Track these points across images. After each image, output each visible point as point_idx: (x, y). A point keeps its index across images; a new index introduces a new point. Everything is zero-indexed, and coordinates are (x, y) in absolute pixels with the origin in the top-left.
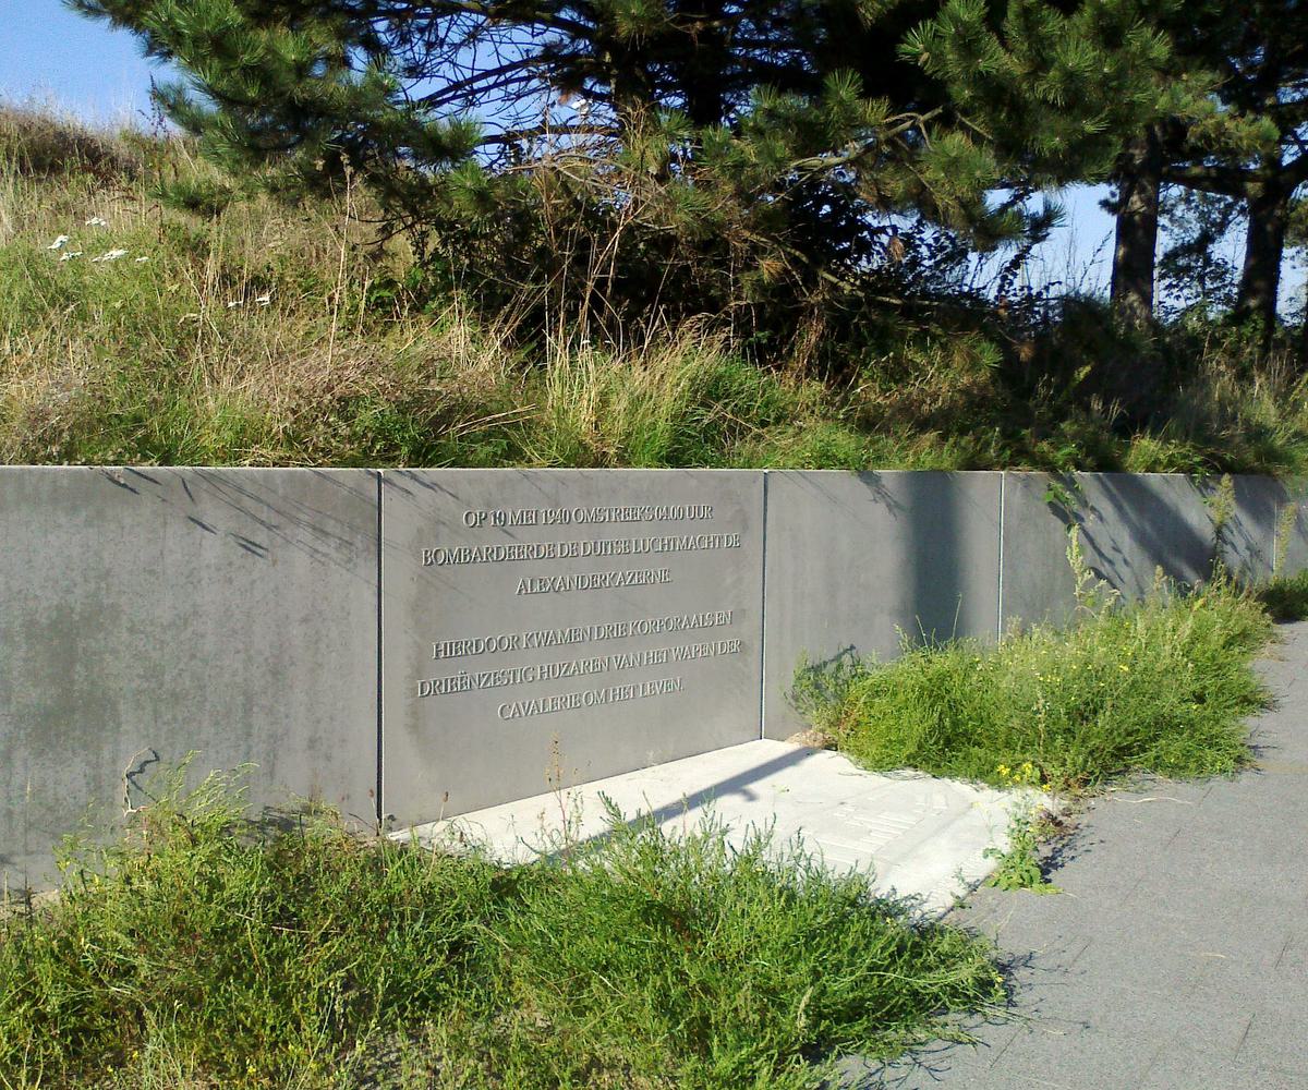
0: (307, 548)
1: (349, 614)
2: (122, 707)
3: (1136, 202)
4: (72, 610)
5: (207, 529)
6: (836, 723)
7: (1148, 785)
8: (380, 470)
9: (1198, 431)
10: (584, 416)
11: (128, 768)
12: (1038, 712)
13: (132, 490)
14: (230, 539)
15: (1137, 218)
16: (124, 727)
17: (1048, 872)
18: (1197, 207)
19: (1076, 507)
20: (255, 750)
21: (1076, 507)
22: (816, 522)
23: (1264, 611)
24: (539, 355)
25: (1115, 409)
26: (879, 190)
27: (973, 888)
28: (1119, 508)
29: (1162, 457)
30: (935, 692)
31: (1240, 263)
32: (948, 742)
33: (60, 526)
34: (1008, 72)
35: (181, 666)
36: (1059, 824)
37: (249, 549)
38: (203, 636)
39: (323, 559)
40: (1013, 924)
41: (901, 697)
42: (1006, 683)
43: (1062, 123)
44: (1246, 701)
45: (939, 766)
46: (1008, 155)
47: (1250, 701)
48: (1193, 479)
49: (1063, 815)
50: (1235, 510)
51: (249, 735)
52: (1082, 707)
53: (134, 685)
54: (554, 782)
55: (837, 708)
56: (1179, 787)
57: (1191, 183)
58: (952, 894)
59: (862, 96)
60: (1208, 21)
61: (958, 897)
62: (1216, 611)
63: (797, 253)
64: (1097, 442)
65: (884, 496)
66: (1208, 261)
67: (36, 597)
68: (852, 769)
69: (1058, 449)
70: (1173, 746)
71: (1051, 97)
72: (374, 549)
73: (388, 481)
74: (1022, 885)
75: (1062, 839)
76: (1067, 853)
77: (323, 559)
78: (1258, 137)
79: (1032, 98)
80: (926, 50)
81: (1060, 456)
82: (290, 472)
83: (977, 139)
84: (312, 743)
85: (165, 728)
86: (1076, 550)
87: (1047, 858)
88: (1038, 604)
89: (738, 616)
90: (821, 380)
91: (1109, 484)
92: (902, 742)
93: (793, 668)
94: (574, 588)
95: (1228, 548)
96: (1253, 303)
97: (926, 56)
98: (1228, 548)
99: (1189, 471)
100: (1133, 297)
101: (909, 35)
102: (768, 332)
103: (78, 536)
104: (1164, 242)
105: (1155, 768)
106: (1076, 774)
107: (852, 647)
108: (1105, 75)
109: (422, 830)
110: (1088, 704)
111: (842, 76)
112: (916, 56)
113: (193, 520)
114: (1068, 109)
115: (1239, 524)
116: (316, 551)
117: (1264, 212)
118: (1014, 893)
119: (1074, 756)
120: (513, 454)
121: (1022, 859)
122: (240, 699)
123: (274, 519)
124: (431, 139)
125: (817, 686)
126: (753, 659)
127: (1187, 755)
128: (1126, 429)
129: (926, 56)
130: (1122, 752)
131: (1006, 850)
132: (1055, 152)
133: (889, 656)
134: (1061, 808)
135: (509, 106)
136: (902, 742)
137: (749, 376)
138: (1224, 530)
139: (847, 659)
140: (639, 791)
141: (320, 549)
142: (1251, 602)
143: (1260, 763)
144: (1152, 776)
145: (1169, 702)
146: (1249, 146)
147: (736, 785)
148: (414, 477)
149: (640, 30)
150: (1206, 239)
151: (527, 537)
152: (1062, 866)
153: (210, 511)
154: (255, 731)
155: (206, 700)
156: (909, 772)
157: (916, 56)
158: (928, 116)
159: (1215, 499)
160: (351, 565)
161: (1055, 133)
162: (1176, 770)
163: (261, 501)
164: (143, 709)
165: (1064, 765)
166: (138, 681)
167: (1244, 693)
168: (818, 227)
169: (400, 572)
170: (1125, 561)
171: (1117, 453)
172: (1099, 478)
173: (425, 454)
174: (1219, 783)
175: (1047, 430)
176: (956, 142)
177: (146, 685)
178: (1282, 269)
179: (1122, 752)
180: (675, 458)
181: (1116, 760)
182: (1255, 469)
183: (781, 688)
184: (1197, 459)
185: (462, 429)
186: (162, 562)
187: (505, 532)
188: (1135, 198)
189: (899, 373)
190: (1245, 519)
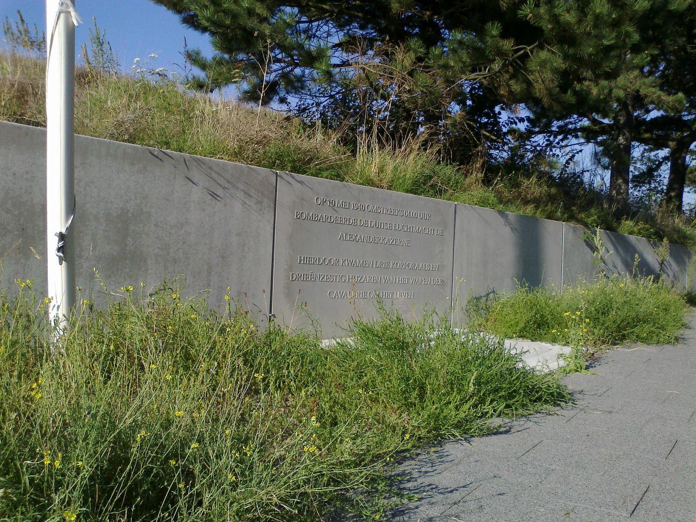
2: (149, 262)
4: (128, 211)
13: (160, 160)
14: (205, 190)
15: (621, 146)
16: (149, 271)
18: (646, 163)
34: (568, 21)
37: (213, 196)
40: (571, 383)
48: (649, 241)
50: (668, 258)
53: (155, 252)
60: (657, 27)
63: (472, 123)
65: (510, 224)
67: (112, 202)
69: (589, 218)
72: (272, 206)
73: (281, 177)
74: (577, 371)
77: (248, 208)
78: (676, 101)
80: (531, 12)
81: (590, 220)
82: (235, 165)
90: (482, 173)
94: (365, 241)
96: (673, 194)
97: (531, 15)
99: (648, 237)
102: (460, 151)
111: (493, 24)
112: (526, 16)
113: (187, 178)
116: (246, 203)
120: (339, 177)
122: (206, 267)
123: (227, 185)
124: (307, 52)
126: (448, 289)
129: (531, 15)
132: (590, 55)
133: (509, 292)
137: (448, 170)
141: (247, 202)
146: (673, 105)
148: (293, 177)
153: (196, 175)
154: (212, 284)
157: (526, 16)
158: (531, 47)
160: (261, 212)
162: (644, 340)
163: (221, 176)
164: (159, 264)
166: (157, 250)
169: (284, 218)
171: (615, 225)
173: (295, 170)
176: (544, 55)
178: (684, 195)
187: (334, 209)
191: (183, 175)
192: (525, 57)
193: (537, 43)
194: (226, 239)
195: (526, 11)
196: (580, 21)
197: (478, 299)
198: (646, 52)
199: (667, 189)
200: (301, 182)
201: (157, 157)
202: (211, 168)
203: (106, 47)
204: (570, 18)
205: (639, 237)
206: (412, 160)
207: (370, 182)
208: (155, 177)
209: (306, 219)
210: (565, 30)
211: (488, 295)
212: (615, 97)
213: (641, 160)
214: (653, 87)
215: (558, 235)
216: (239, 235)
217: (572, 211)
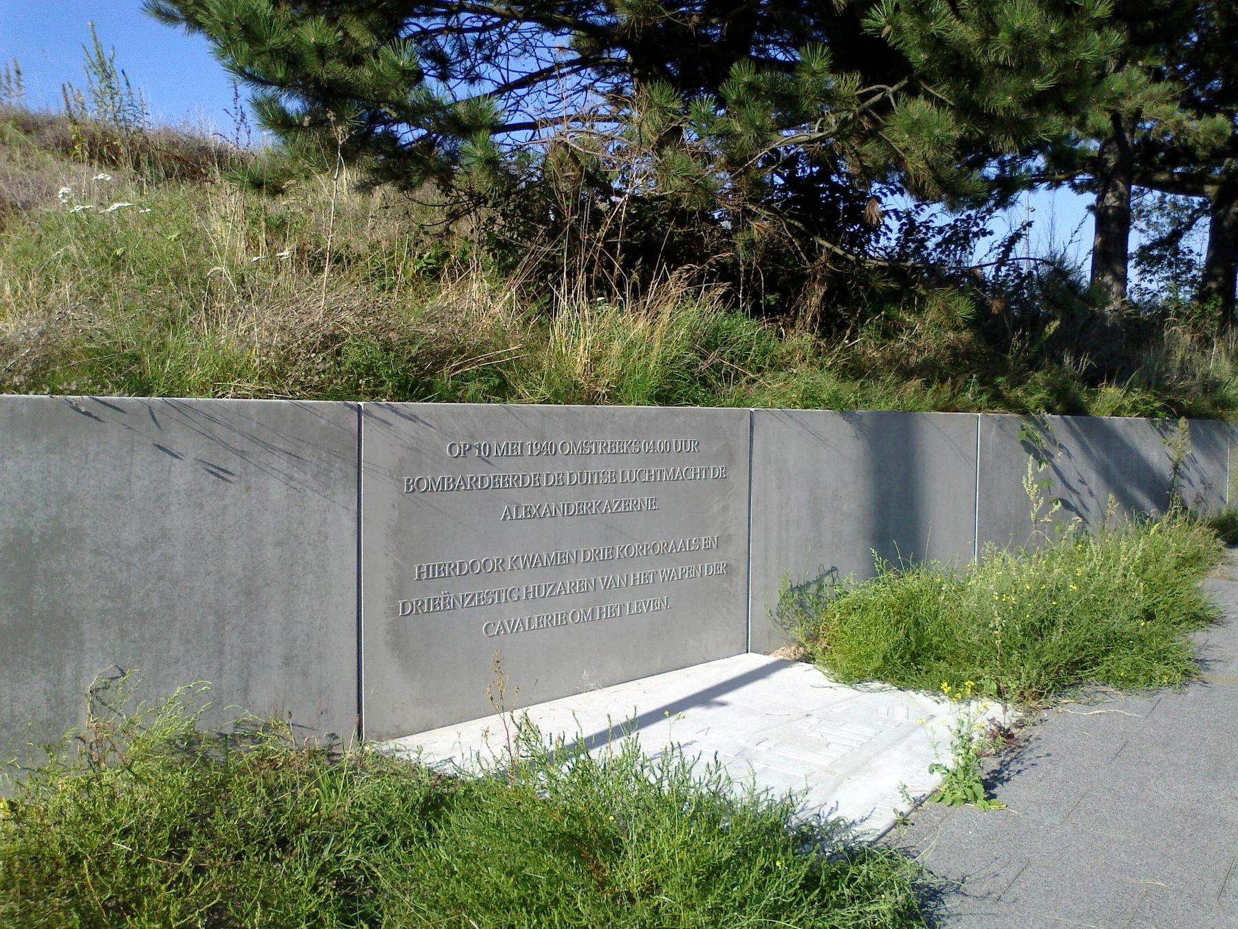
0: (281, 476)
1: (326, 538)
2: (86, 626)
3: (1111, 200)
4: (31, 532)
5: (176, 457)
6: (813, 638)
7: (1100, 697)
8: (361, 403)
9: (1155, 383)
10: (581, 358)
11: (92, 682)
12: (995, 628)
13: (96, 418)
14: (200, 466)
15: (1110, 211)
17: (995, 786)
18: (1169, 214)
19: (1045, 444)
20: (227, 668)
21: (1045, 444)
22: (793, 453)
23: (1217, 536)
24: (550, 309)
25: (1085, 362)
26: (861, 161)
27: (918, 803)
28: (1084, 448)
29: (1126, 402)
30: (906, 610)
31: (1201, 261)
32: (914, 656)
33: (18, 452)
35: (149, 586)
36: (1011, 736)
38: (172, 558)
39: (299, 486)
41: (872, 615)
42: (969, 604)
43: (1013, 83)
44: (1196, 617)
45: (903, 679)
46: (966, 115)
47: (1200, 618)
49: (1016, 727)
51: (221, 653)
52: (1038, 624)
53: (98, 605)
54: (497, 702)
55: (813, 627)
56: (1130, 699)
57: (1164, 187)
58: (895, 810)
59: (834, 69)
61: (901, 814)
62: (1168, 537)
64: (1066, 390)
66: (1176, 252)
68: (825, 681)
70: (1122, 662)
71: (1001, 59)
72: (354, 476)
73: (368, 414)
74: (966, 801)
75: (1012, 751)
76: (1014, 767)
77: (299, 486)
79: (986, 61)
80: (889, 23)
81: (1032, 401)
83: (940, 104)
84: (288, 660)
85: (133, 646)
86: (1031, 480)
87: (994, 771)
88: (1007, 530)
89: (725, 540)
91: (1073, 423)
92: (869, 656)
93: (778, 588)
95: (1184, 482)
96: (1213, 285)
97: (888, 28)
98: (1184, 482)
99: (1151, 415)
100: (1108, 279)
101: (873, 11)
102: (768, 288)
103: (38, 463)
104: (1136, 240)
105: (1106, 681)
106: (1030, 687)
107: (834, 569)
108: (1052, 36)
109: (402, 742)
110: (1043, 621)
113: (159, 447)
114: (1018, 70)
115: (1193, 460)
116: (292, 478)
117: (1221, 211)
118: (959, 809)
119: (1030, 671)
120: (502, 391)
121: (966, 774)
123: (247, 446)
125: (802, 604)
126: (740, 581)
127: (1136, 668)
128: (1092, 380)
129: (888, 28)
130: (1076, 666)
131: (951, 766)
132: (1008, 110)
134: (1014, 720)
135: (554, 105)
136: (869, 656)
137: (745, 328)
138: (1181, 466)
139: (828, 580)
140: (562, 719)
141: (296, 475)
142: (1205, 529)
143: (1206, 675)
144: (1104, 689)
145: (1120, 621)
146: (1205, 140)
147: (705, 698)
148: (395, 411)
149: (638, 21)
150: (1176, 235)
151: (511, 467)
152: (1008, 780)
153: (178, 438)
154: (227, 649)
155: (175, 619)
156: (878, 684)
158: (896, 87)
159: (1171, 440)
161: (1007, 93)
162: (1127, 683)
165: (1019, 679)
166: (102, 601)
167: (1194, 609)
168: (824, 205)
169: (380, 494)
170: (1091, 493)
171: (1084, 398)
172: (1065, 420)
174: (1167, 696)
175: (1018, 380)
176: (919, 107)
177: (110, 605)
179: (1076, 666)
180: (663, 397)
181: (1070, 675)
182: (1206, 412)
183: (766, 606)
184: (1157, 405)
185: (457, 369)
186: (131, 489)
188: (1109, 195)
189: (889, 332)
190: (1198, 456)
191: (150, 443)
192: (884, 107)
193: (906, 82)
194: (252, 557)
195: (878, 19)
196: (985, 41)
197: (801, 589)
198: (1140, 63)
199: (1204, 276)
200: (413, 418)
201: (86, 413)
202: (211, 418)
203: (118, 81)
204: (965, 33)
205: (1133, 418)
206: (668, 319)
207: (570, 393)
208: (87, 456)
209: (429, 489)
210: (958, 57)
211: (822, 577)
212: (1093, 126)
213: (1160, 208)
214: (1168, 102)
215: (963, 446)
216: (279, 544)
217: (996, 387)
